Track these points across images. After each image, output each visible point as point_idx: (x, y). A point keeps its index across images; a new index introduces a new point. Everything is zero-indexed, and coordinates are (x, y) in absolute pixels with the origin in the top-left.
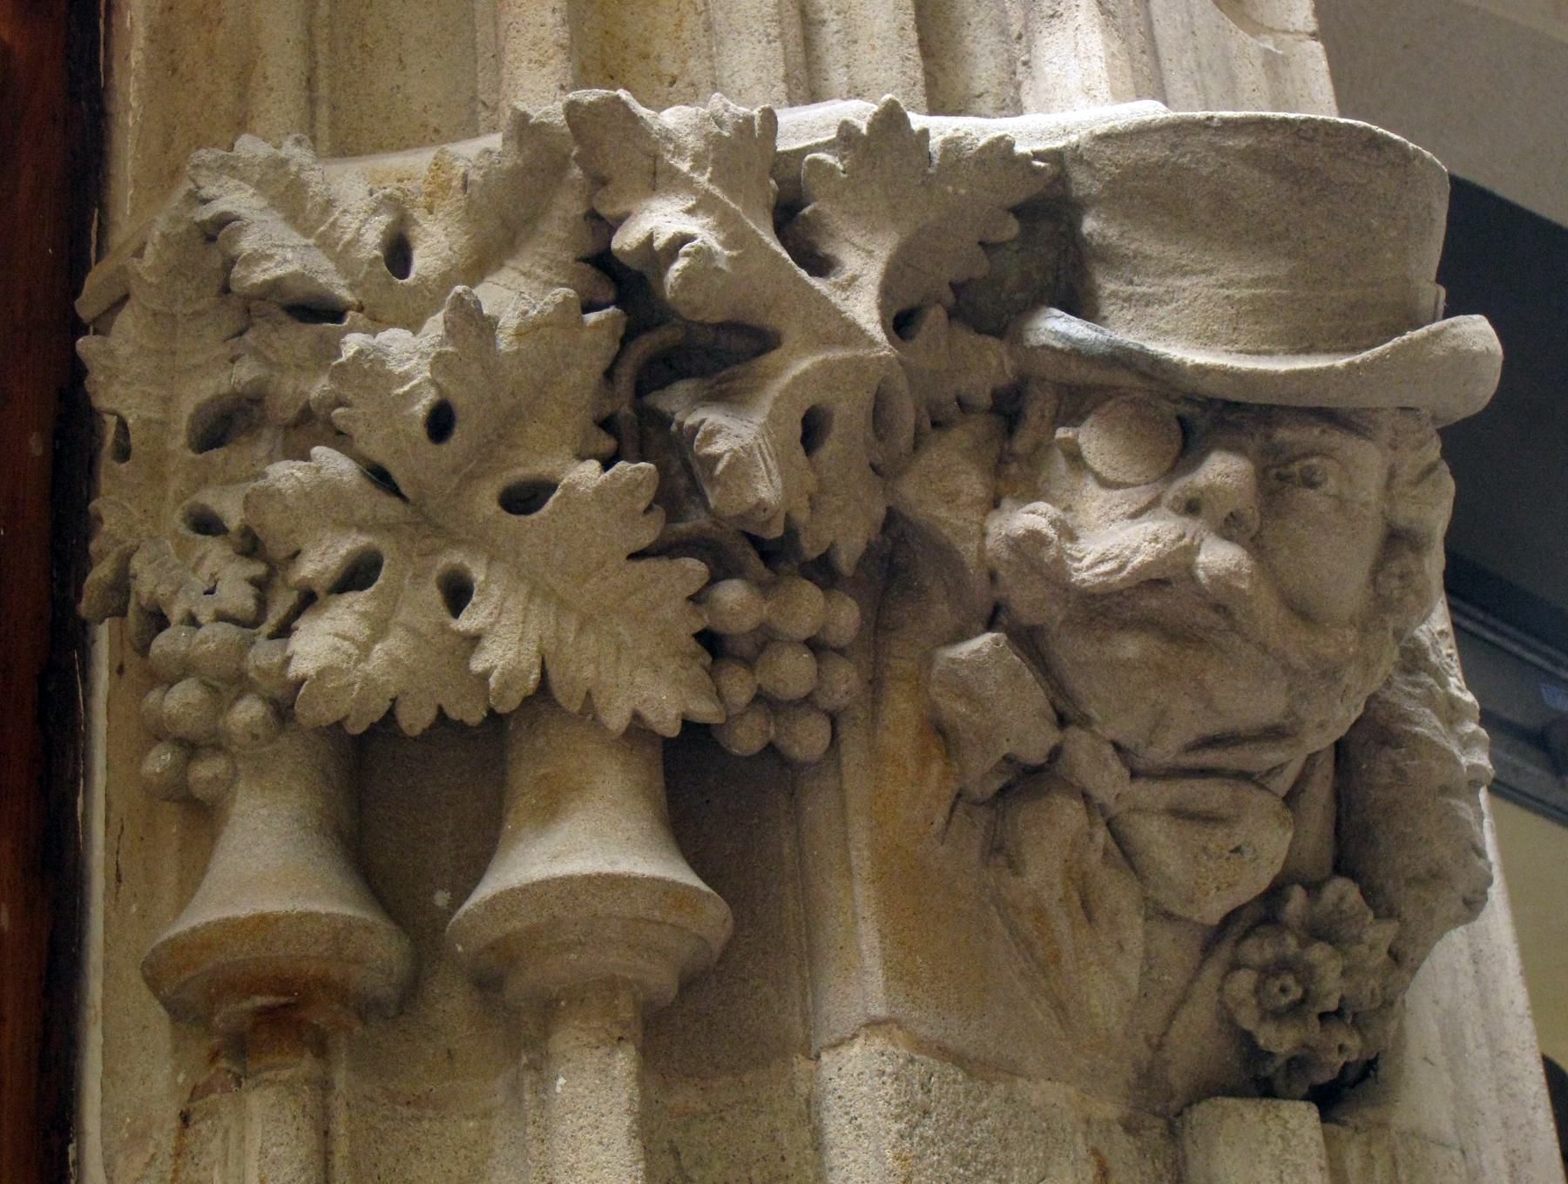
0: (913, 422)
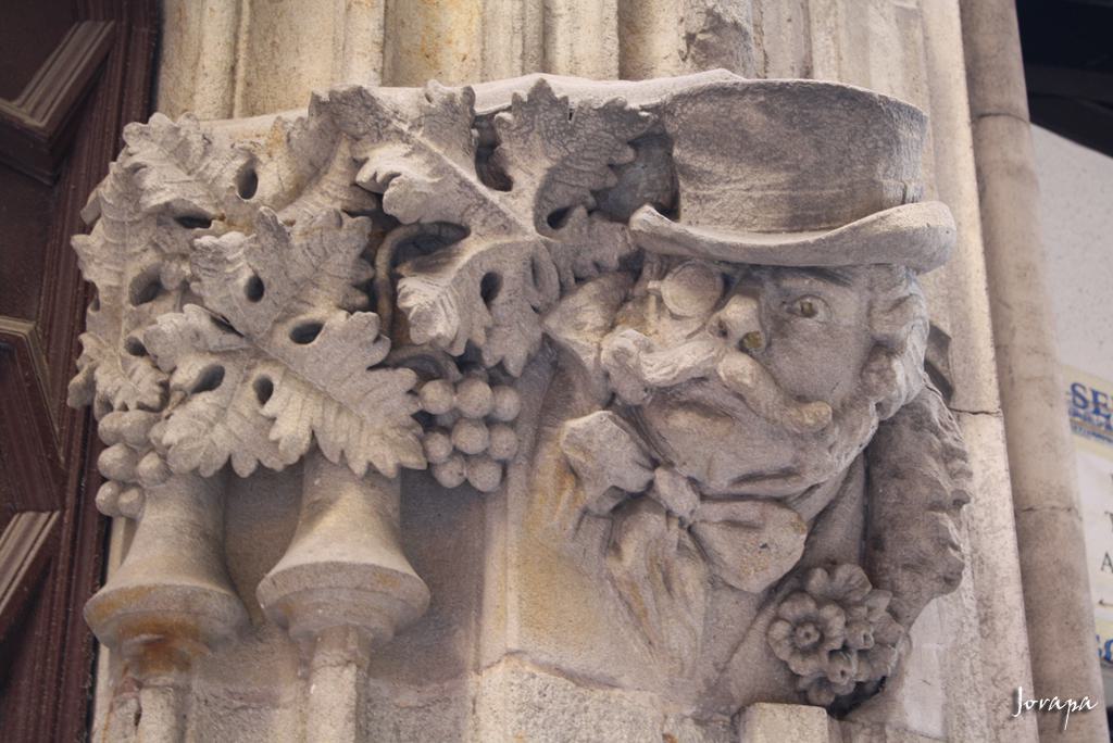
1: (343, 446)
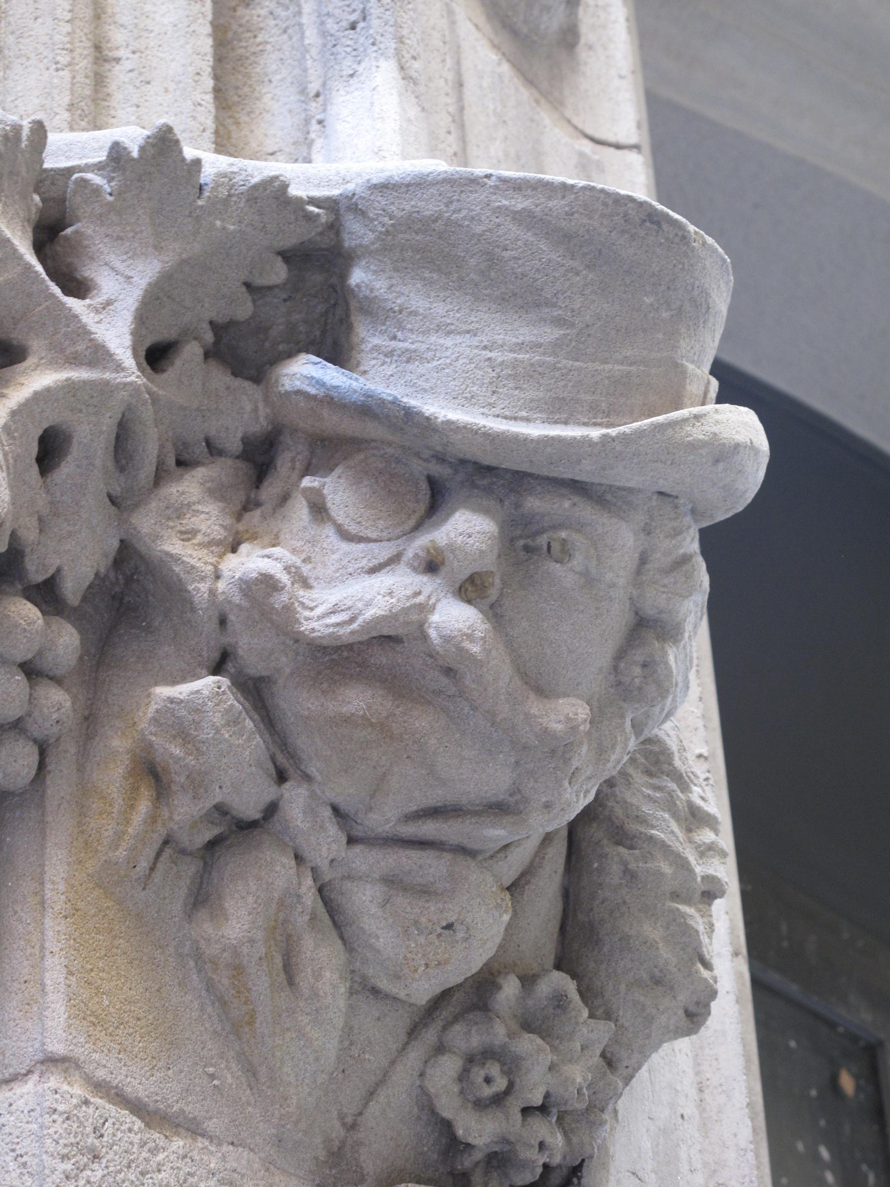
0: (155, 455)
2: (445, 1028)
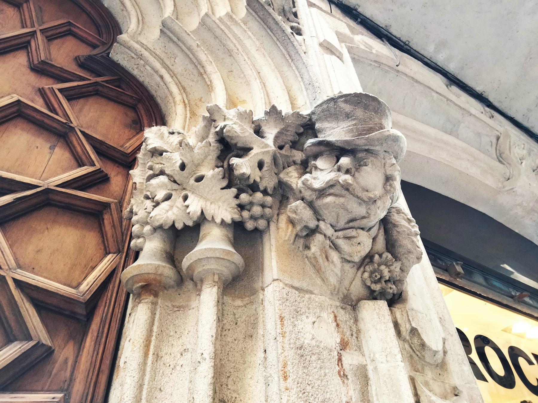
1: (212, 214)
2: (364, 267)
